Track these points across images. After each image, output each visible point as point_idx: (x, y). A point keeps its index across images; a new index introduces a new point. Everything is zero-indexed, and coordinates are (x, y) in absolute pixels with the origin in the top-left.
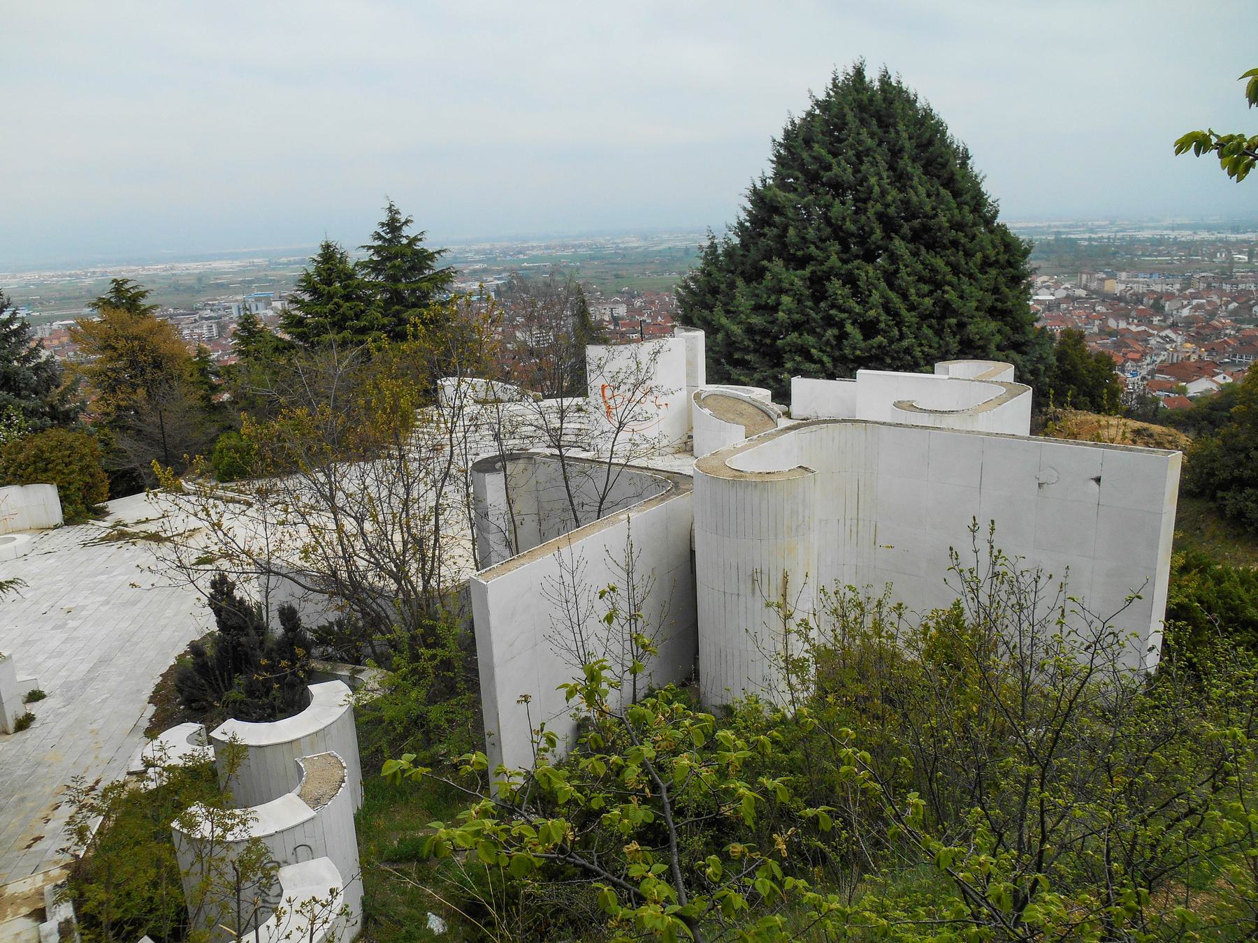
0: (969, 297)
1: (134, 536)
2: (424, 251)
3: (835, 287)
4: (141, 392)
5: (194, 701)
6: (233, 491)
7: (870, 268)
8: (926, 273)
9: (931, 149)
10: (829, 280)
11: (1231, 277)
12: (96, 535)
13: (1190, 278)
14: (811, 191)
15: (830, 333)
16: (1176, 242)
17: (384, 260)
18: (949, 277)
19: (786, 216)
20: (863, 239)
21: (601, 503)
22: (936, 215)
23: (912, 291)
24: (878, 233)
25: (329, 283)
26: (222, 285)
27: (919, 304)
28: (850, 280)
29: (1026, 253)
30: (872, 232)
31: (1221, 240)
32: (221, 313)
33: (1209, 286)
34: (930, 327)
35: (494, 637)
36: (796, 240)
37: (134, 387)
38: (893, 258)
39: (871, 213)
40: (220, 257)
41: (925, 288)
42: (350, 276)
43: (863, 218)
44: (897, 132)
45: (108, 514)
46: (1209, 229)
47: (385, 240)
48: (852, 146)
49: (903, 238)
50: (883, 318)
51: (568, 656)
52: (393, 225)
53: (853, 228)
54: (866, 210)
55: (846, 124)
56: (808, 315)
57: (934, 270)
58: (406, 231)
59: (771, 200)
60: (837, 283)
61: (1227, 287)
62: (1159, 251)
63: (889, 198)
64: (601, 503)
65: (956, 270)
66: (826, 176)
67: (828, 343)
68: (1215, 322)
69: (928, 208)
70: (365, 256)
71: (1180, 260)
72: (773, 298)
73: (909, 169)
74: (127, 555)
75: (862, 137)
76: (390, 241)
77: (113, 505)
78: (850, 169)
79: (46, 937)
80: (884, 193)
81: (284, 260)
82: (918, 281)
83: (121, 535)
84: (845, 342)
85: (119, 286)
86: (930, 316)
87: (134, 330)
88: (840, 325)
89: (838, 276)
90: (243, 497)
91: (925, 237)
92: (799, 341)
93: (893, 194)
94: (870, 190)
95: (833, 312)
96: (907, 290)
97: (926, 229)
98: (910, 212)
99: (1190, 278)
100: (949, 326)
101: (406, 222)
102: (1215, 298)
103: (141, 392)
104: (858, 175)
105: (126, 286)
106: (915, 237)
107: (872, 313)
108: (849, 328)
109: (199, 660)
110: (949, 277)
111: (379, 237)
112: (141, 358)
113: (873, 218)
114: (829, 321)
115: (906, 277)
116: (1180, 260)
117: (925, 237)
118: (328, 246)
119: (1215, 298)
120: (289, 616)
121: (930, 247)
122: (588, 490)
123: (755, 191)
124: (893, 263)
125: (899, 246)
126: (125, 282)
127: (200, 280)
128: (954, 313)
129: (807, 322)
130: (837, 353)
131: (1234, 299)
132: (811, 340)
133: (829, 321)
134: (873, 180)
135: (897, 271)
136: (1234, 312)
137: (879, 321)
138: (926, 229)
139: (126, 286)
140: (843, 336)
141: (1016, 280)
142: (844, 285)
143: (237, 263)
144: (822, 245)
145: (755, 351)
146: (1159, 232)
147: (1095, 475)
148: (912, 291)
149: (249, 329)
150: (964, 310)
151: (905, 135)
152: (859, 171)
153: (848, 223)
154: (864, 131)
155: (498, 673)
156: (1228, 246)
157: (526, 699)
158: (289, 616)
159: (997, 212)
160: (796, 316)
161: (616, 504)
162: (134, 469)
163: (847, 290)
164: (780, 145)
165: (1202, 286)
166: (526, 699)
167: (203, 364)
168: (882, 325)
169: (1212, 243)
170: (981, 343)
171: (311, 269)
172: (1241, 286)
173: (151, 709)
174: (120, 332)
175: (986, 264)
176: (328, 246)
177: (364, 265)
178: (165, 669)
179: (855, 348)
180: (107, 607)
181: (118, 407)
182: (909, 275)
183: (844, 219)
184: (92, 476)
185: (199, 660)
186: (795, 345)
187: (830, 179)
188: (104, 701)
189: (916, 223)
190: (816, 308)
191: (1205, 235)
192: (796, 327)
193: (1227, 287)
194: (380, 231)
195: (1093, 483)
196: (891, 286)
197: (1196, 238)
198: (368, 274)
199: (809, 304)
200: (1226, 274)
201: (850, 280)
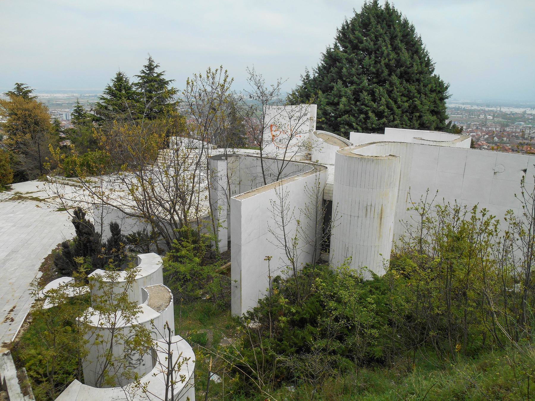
0: (424, 105)
1: (26, 198)
2: (164, 79)
3: (365, 96)
4: (28, 136)
5: (64, 269)
6: (74, 181)
7: (381, 88)
8: (406, 92)
9: (408, 37)
10: (361, 92)
11: (486, 125)
12: (7, 197)
13: (469, 124)
14: (354, 53)
15: (362, 116)
16: (464, 109)
17: (145, 82)
18: (416, 94)
19: (342, 63)
20: (378, 74)
21: (279, 175)
22: (412, 66)
23: (399, 99)
24: (386, 72)
25: (120, 91)
26: (59, 104)
27: (402, 105)
28: (372, 93)
29: (447, 88)
30: (383, 72)
31: (482, 110)
32: (58, 116)
33: (477, 128)
34: (407, 116)
35: (243, 229)
36: (346, 74)
37: (25, 133)
38: (392, 84)
39: (383, 63)
40: (59, 92)
41: (405, 99)
42: (130, 88)
43: (379, 65)
44: (394, 29)
45: (12, 189)
46: (478, 105)
47: (146, 74)
48: (373, 33)
49: (396, 76)
50: (386, 110)
51: (276, 242)
52: (150, 67)
53: (374, 70)
54: (380, 62)
55: (370, 23)
56: (352, 108)
57: (409, 92)
58: (157, 70)
59: (335, 56)
60: (365, 93)
61: (484, 129)
62: (458, 113)
63: (391, 57)
64: (279, 175)
65: (419, 92)
66: (361, 46)
67: (360, 121)
68: (479, 143)
69: (408, 63)
70: (137, 80)
71: (466, 117)
72: (337, 99)
73: (399, 45)
74: (23, 206)
75: (378, 29)
76: (148, 74)
77: (14, 186)
78: (372, 43)
79: (9, 380)
80: (388, 55)
81: (87, 95)
82: (402, 95)
83: (19, 197)
84: (368, 121)
85: (19, 87)
86: (406, 112)
87: (26, 106)
88: (366, 113)
89: (366, 91)
90: (79, 184)
91: (406, 76)
92: (348, 119)
93: (393, 55)
94: (382, 53)
95: (363, 107)
96: (397, 99)
97: (406, 73)
98: (399, 63)
99: (469, 124)
100: (416, 116)
101: (157, 66)
102: (479, 133)
103: (28, 136)
104: (376, 46)
105: (22, 87)
106: (401, 77)
107: (382, 108)
108: (370, 114)
109: (66, 250)
110: (416, 94)
111: (144, 72)
112: (29, 120)
113: (383, 66)
114: (361, 112)
115: (396, 93)
116: (466, 117)
117: (406, 76)
118: (120, 74)
119: (479, 133)
120: (115, 228)
121: (407, 81)
122: (274, 168)
123: (329, 52)
124: (391, 87)
125: (394, 79)
126: (22, 84)
127: (49, 101)
128: (418, 110)
129: (351, 110)
130: (364, 126)
131: (487, 134)
132: (353, 119)
133: (361, 112)
134: (384, 48)
135: (392, 90)
136: (486, 139)
137: (384, 112)
138: (406, 73)
139: (22, 87)
140: (367, 118)
141: (442, 99)
142: (368, 95)
143: (66, 95)
144: (359, 77)
145: (326, 123)
146: (457, 105)
147: (524, 168)
148: (399, 99)
149: (79, 113)
150: (423, 109)
151: (398, 30)
152: (377, 44)
153: (371, 68)
154: (379, 26)
155: (243, 249)
156: (485, 112)
157: (269, 259)
158: (115, 228)
159: (434, 69)
160: (348, 108)
161: (286, 176)
162: (24, 171)
163: (369, 97)
164: (340, 32)
165: (475, 128)
166: (269, 259)
167: (57, 123)
168: (386, 114)
169: (479, 111)
170: (429, 125)
171: (111, 84)
172: (490, 129)
173: (40, 274)
174: (19, 106)
175: (432, 91)
176: (120, 74)
177: (136, 85)
178: (46, 256)
179: (372, 124)
180: (14, 228)
181: (17, 142)
182: (398, 92)
183: (370, 66)
184: (5, 170)
185: (66, 250)
186: (346, 121)
187: (363, 48)
188: (15, 270)
189: (402, 69)
190: (355, 105)
191: (475, 107)
192: (346, 112)
193: (484, 129)
194: (144, 69)
195: (523, 172)
196: (390, 96)
197: (473, 108)
198: (139, 88)
199: (353, 102)
200: (484, 124)
201: (372, 93)
